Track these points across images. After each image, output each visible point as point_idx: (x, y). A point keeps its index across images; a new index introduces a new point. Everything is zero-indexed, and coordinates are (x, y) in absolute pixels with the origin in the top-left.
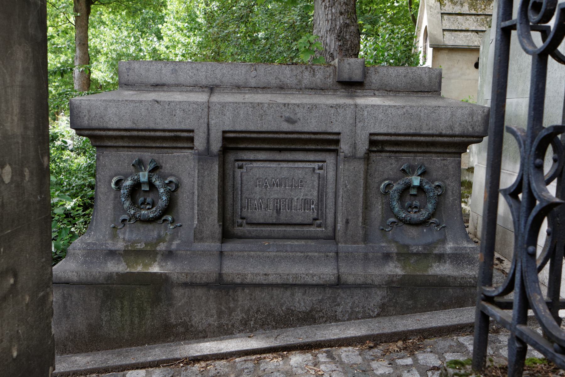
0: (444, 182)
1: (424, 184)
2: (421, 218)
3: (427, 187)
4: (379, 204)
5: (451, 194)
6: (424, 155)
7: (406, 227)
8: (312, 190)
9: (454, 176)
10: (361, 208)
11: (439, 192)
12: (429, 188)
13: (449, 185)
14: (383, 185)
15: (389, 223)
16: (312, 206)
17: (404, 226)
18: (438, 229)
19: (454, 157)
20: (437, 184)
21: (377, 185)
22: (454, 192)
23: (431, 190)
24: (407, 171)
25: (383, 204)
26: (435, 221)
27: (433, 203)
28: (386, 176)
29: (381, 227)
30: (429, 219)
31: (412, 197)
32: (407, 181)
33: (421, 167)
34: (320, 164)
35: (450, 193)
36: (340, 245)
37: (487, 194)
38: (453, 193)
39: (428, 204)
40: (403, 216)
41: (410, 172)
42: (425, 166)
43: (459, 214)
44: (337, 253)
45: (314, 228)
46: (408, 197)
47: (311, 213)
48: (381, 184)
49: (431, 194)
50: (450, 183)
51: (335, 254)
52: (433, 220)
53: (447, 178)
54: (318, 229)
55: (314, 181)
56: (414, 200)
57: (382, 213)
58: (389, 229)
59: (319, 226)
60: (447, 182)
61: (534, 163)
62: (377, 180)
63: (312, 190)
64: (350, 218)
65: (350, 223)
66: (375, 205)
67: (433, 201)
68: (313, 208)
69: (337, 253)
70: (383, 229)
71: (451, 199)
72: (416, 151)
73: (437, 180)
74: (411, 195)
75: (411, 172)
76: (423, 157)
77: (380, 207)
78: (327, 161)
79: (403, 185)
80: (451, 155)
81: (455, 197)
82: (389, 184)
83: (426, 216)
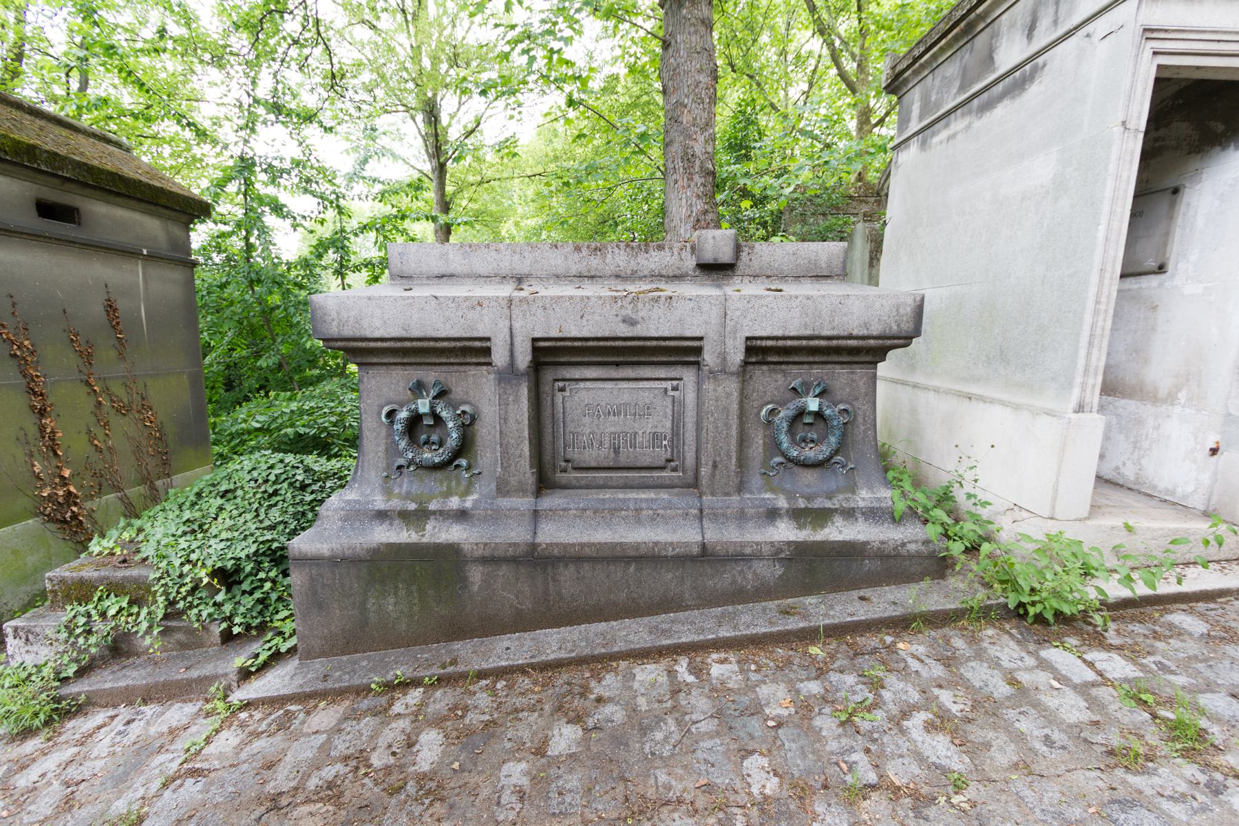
0: (852, 405)
5: (862, 421)
7: (796, 470)
14: (764, 410)
20: (842, 407)
21: (756, 410)
24: (799, 390)
25: (765, 436)
29: (763, 471)
31: (806, 427)
32: (800, 404)
34: (675, 383)
35: (860, 420)
44: (701, 511)
46: (801, 426)
49: (835, 423)
52: (838, 458)
53: (857, 399)
54: (674, 474)
55: (666, 407)
62: (756, 404)
64: (718, 459)
67: (838, 433)
68: (665, 446)
69: (701, 511)
73: (840, 402)
74: (805, 424)
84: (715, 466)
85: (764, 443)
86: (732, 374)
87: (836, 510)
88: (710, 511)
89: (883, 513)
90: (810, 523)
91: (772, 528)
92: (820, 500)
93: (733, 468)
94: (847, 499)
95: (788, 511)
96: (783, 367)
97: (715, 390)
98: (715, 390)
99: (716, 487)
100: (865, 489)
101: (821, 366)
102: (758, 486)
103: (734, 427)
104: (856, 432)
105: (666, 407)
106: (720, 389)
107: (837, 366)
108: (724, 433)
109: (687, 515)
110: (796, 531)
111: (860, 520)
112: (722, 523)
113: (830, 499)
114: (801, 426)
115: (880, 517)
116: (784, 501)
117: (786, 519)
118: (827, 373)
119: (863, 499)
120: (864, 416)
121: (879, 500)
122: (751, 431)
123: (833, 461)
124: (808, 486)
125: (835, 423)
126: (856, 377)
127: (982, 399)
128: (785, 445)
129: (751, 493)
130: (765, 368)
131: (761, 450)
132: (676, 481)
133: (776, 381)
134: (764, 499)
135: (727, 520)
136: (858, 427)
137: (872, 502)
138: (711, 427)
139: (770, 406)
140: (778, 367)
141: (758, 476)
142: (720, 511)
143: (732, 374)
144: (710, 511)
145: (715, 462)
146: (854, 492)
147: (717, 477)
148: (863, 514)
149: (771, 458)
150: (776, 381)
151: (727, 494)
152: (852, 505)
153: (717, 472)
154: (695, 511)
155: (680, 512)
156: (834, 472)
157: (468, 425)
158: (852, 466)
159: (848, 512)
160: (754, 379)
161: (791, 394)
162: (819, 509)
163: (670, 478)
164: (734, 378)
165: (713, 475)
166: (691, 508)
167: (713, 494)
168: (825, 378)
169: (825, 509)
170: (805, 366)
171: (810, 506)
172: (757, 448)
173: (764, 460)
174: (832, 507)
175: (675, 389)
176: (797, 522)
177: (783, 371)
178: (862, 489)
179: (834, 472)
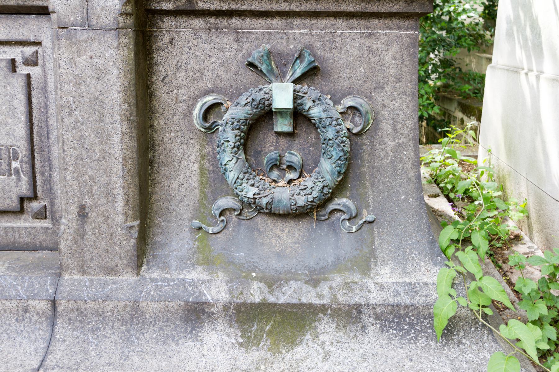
0: (370, 98)
1: (309, 104)
2: (301, 201)
3: (316, 112)
4: (193, 158)
5: (390, 130)
6: (314, 21)
7: (261, 222)
8: (10, 121)
9: (399, 80)
10: (120, 173)
11: (356, 125)
12: (324, 115)
13: (384, 106)
14: (199, 106)
15: (217, 213)
16: (15, 164)
17: (259, 219)
18: (354, 229)
19: (399, 28)
20: (349, 102)
21: (183, 107)
22: (399, 125)
23: (328, 122)
24: (263, 67)
25: (203, 157)
26: (345, 205)
27: (335, 157)
28: (206, 83)
29: (197, 223)
30: (329, 200)
31: (282, 140)
32: (260, 96)
33: (300, 56)
34: (29, 50)
35: (386, 127)
36: (66, 277)
37: (131, 77)
38: (395, 130)
39: (322, 160)
40: (250, 195)
41: (271, 71)
42: (313, 54)
43: (412, 186)
44: (54, 303)
45: (26, 220)
46: (271, 138)
47: (13, 184)
48: (194, 105)
49: (330, 133)
50: (386, 102)
51: (49, 307)
52: (341, 202)
53: (379, 87)
54: (39, 224)
55: (13, 96)
56: (288, 149)
57: (201, 183)
58: (216, 229)
59: (41, 215)
60: (378, 97)
61: (426, 144)
62: (183, 94)
63: (10, 121)
64: (88, 201)
65: (93, 215)
66: (180, 161)
67: (335, 153)
68: (17, 171)
69: (54, 303)
70: (200, 228)
71: (392, 144)
72: (287, 9)
73: (349, 93)
74: (279, 134)
75: (276, 71)
76: (311, 28)
77: (196, 167)
78: (44, 44)
79: (248, 109)
80: (388, 22)
81: (403, 140)
82: (215, 106)
83: (315, 194)
84: (83, 214)
85: (202, 170)
86: (106, 30)
87: (323, 309)
88: (71, 305)
89: (418, 316)
90: (270, 333)
91: (190, 343)
92: (294, 285)
93: (120, 219)
94: (348, 286)
95: (226, 308)
96: (235, 22)
97: (72, 62)
98: (72, 62)
99: (87, 255)
100: (391, 264)
101: (307, 21)
102: (183, 252)
103: (117, 138)
104: (379, 151)
105: (13, 96)
106: (82, 60)
107: (340, 23)
108: (97, 149)
109: (26, 311)
110: (237, 352)
111: (371, 329)
112: (92, 331)
113: (315, 283)
114: (271, 138)
115: (411, 325)
116: (224, 288)
117: (221, 324)
118: (320, 36)
119: (381, 287)
120: (395, 122)
121: (412, 288)
122: (175, 147)
123: (331, 207)
124: (280, 256)
125: (330, 133)
126: (377, 45)
127: (503, 65)
128: (231, 176)
129: (165, 267)
130: (198, 23)
131: (195, 182)
132: (41, 237)
133: (222, 50)
134: (183, 282)
135: (105, 324)
136: (382, 142)
137: (397, 294)
138: (69, 137)
139: (210, 99)
140: (224, 22)
141: (186, 233)
142: (92, 305)
143: (106, 30)
144: (71, 305)
145: (82, 207)
146: (366, 270)
147: (89, 236)
148: (377, 317)
149: (215, 199)
150: (222, 50)
151: (111, 270)
152: (357, 300)
153: (88, 227)
154: (43, 305)
155: (12, 305)
156: (334, 228)
157: (359, 134)
158: (370, 218)
159: (348, 314)
160: (178, 44)
161: (251, 75)
162: (289, 305)
163: (29, 231)
164: (110, 38)
165: (81, 234)
166: (34, 298)
167: (82, 270)
168: (317, 44)
169: (301, 306)
170: (278, 22)
171: (271, 299)
172: (188, 178)
173: (201, 204)
174: (316, 301)
175: (32, 62)
176: (244, 331)
177: (236, 31)
178: (385, 263)
179: (334, 228)
